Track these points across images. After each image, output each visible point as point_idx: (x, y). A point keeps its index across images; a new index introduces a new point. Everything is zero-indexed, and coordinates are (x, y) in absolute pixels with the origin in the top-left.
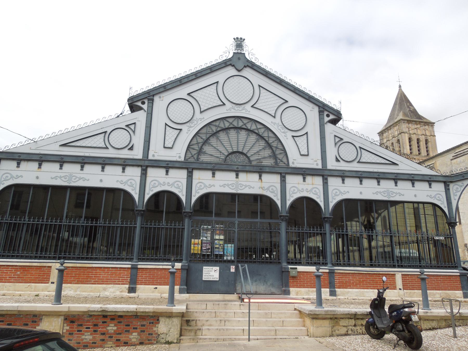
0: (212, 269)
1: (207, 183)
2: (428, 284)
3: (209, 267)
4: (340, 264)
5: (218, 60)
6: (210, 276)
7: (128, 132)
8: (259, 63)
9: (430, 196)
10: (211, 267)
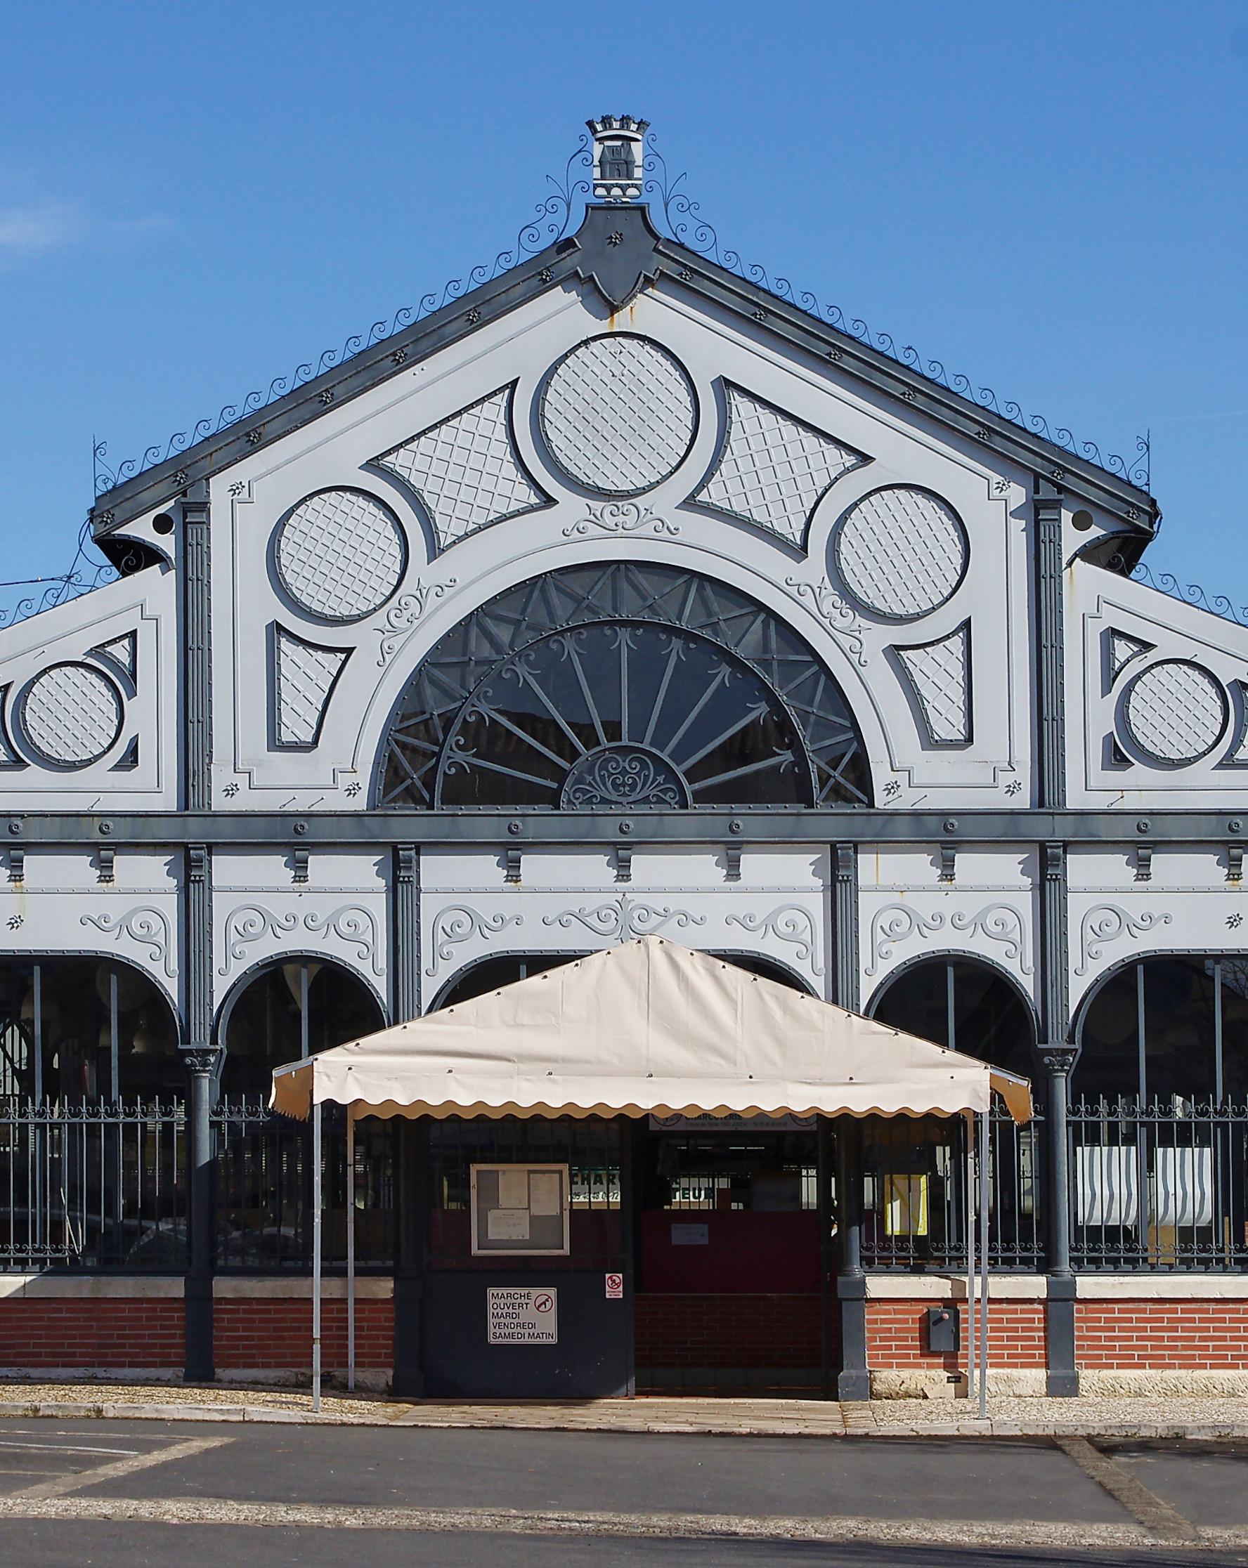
0: (528, 1296)
1: (485, 907)
2: (177, 1327)
3: (512, 1291)
4: (1220, 1261)
5: (514, 255)
6: (518, 1325)
7: (1138, 677)
8: (721, 254)
9: (745, 923)
10: (524, 1291)
